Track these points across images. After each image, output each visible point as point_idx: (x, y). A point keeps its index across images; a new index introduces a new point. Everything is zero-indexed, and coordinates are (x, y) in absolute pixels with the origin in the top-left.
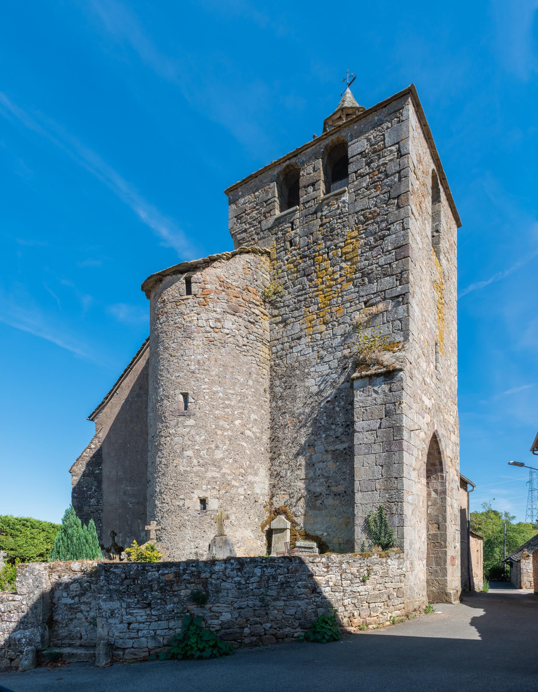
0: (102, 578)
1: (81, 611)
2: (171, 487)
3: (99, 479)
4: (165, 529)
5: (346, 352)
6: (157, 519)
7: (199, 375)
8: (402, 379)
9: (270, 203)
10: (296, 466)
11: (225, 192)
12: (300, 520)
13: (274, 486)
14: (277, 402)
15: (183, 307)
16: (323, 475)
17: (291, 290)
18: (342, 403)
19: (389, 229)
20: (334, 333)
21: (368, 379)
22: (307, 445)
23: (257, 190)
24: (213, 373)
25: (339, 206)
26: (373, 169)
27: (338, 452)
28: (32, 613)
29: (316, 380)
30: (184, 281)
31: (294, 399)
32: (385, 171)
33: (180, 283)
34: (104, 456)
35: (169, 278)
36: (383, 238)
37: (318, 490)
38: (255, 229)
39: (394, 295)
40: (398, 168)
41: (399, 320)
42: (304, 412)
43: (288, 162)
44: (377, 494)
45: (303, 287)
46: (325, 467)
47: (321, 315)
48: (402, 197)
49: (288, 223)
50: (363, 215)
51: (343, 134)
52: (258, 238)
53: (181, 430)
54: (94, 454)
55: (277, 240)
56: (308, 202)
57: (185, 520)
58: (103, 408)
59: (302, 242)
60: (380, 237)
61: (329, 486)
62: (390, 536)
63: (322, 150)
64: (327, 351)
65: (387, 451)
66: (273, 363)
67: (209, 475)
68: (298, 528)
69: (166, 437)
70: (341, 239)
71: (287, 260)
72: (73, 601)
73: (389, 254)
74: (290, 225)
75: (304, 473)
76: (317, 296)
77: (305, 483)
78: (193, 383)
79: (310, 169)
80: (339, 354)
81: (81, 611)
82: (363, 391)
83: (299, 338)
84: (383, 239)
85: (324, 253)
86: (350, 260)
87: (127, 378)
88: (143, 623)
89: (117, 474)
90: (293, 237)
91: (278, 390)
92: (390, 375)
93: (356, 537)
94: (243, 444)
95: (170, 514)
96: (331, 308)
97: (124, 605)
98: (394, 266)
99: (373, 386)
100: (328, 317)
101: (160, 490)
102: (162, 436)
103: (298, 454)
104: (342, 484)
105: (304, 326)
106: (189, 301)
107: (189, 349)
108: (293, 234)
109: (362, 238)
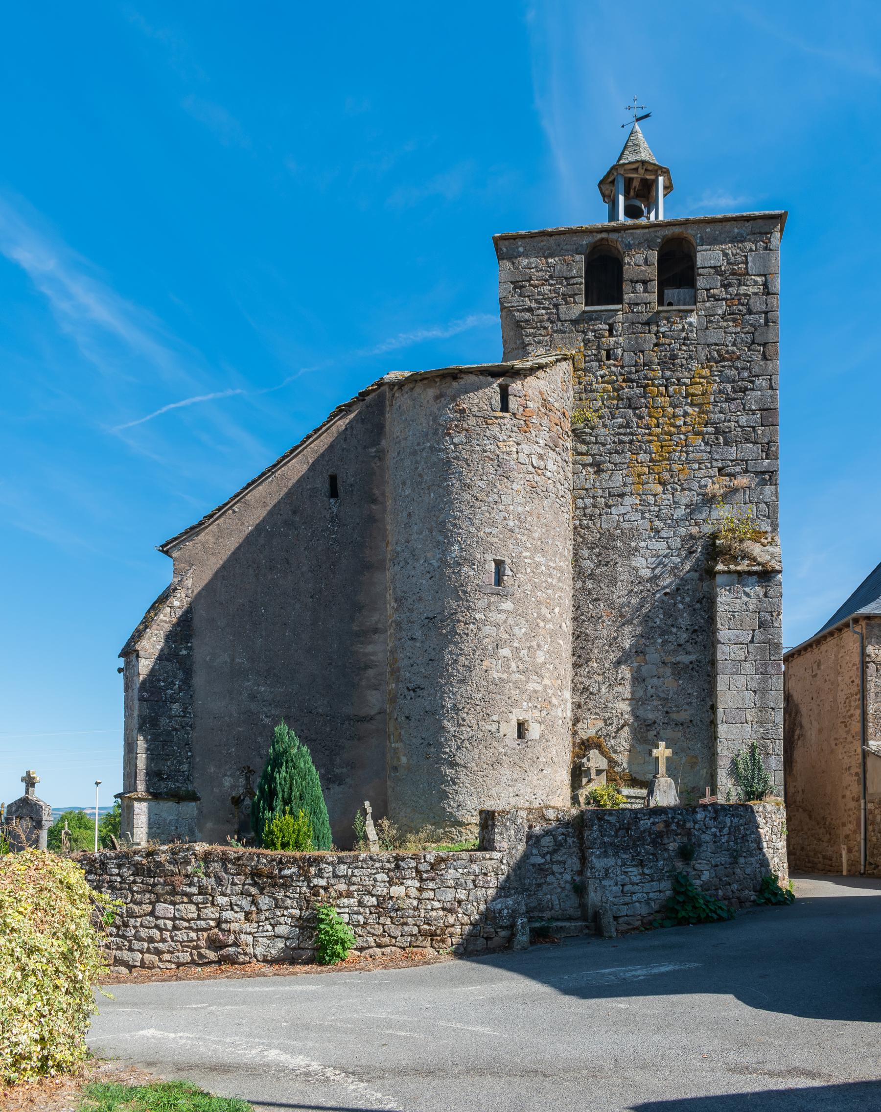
0: (595, 828)
1: (553, 873)
2: (478, 702)
3: (186, 667)
4: (465, 767)
5: (694, 530)
6: (448, 750)
7: (519, 536)
8: (781, 583)
9: (574, 284)
10: (616, 680)
11: (496, 241)
12: (622, 759)
13: (579, 706)
14: (584, 582)
15: (495, 429)
16: (658, 696)
17: (608, 422)
18: (688, 599)
19: (752, 382)
20: (676, 500)
21: (736, 575)
22: (634, 651)
23: (552, 256)
24: (536, 535)
25: (684, 327)
26: (731, 295)
27: (681, 665)
28: (516, 875)
29: (651, 560)
30: (498, 389)
31: (613, 582)
32: (747, 304)
33: (492, 390)
34: (196, 622)
35: (472, 378)
36: (744, 390)
37: (651, 716)
38: (547, 313)
39: (759, 470)
40: (764, 308)
41: (766, 503)
42: (629, 602)
43: (604, 235)
44: (747, 727)
45: (628, 423)
46: (661, 684)
47: (656, 471)
48: (769, 346)
49: (605, 323)
50: (718, 351)
51: (690, 231)
52: (552, 328)
53: (494, 616)
54: (179, 619)
55: (586, 342)
56: (638, 304)
57: (500, 753)
58: (198, 534)
59: (626, 358)
60: (741, 388)
61: (667, 712)
62: (766, 782)
63: (659, 240)
64: (665, 524)
65: (761, 673)
66: (577, 522)
67: (531, 686)
68: (618, 769)
69: (466, 624)
70: (686, 374)
71: (602, 377)
72: (543, 861)
73: (753, 414)
74: (607, 327)
75: (629, 690)
76: (650, 442)
77: (630, 705)
78: (511, 546)
79: (640, 258)
80: (682, 531)
81: (553, 873)
82: (729, 591)
83: (622, 495)
84: (744, 392)
85: (661, 385)
86: (700, 405)
87: (260, 488)
88: (637, 884)
89: (233, 660)
90: (612, 347)
91: (586, 563)
92: (766, 576)
93: (719, 783)
94: (561, 642)
95: (475, 743)
96: (670, 464)
97: (619, 862)
98: (759, 432)
99: (744, 586)
100: (666, 476)
101: (455, 705)
102: (459, 621)
103: (619, 663)
104: (686, 710)
105: (629, 480)
106: (506, 421)
107: (506, 494)
108: (612, 343)
109: (715, 381)
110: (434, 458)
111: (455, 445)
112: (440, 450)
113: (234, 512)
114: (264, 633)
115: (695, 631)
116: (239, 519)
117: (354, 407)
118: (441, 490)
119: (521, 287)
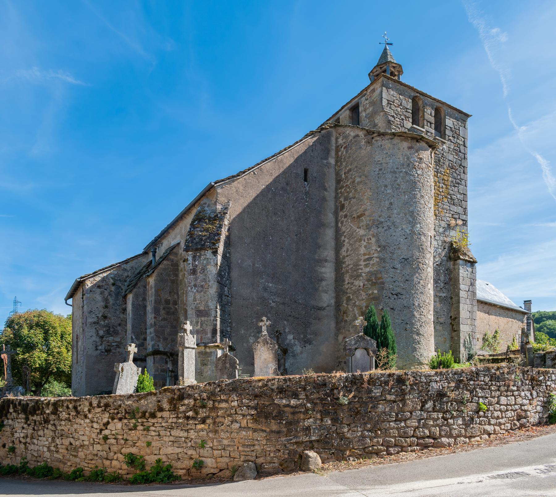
6: (416, 327)
89: (254, 265)
110: (407, 178)
111: (418, 175)
112: (411, 175)
113: (254, 174)
114: (271, 251)
115: (445, 283)
116: (257, 179)
117: (316, 134)
118: (411, 195)
119: (391, 104)
